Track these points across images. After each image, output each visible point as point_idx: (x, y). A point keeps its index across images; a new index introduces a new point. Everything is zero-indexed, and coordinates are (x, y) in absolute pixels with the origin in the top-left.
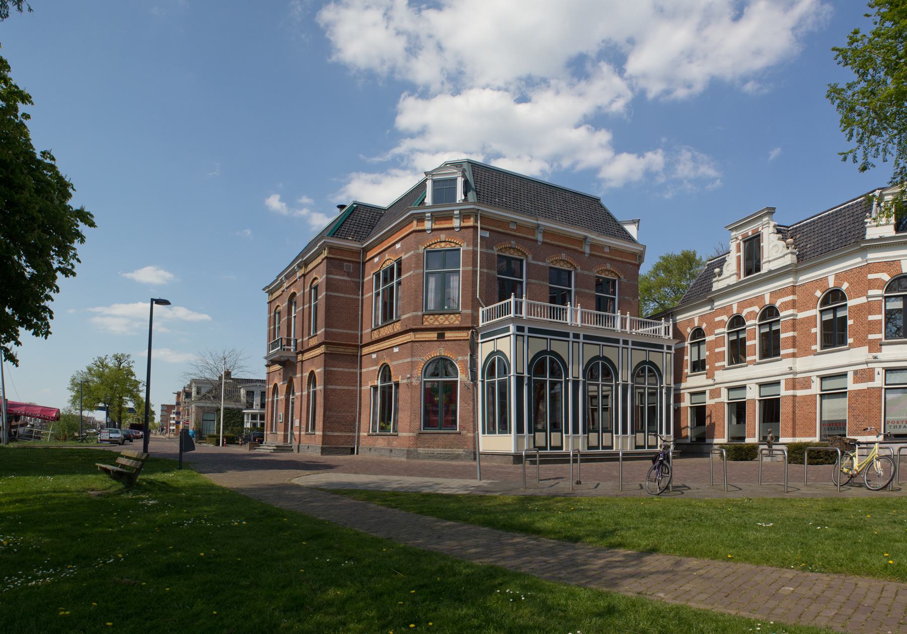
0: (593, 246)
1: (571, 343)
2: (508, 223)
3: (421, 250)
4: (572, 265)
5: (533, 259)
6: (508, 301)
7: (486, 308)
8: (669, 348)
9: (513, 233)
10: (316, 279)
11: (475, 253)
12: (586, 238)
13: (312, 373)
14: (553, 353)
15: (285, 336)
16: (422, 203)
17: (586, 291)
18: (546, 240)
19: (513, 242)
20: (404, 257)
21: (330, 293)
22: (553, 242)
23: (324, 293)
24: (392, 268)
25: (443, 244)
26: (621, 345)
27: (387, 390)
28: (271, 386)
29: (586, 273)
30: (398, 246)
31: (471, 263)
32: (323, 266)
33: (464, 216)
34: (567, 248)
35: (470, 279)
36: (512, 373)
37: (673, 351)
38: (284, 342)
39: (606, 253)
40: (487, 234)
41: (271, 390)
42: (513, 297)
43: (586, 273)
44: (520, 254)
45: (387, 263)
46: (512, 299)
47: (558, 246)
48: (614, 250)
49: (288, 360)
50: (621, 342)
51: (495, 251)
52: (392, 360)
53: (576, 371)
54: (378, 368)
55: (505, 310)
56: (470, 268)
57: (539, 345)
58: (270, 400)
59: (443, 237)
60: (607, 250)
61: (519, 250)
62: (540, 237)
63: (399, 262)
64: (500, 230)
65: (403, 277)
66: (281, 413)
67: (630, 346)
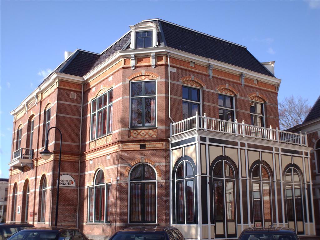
0: (247, 80)
1: (239, 150)
2: (188, 63)
3: (128, 82)
4: (233, 93)
5: (207, 88)
6: (193, 117)
7: (175, 124)
8: (306, 154)
9: (192, 70)
10: (49, 104)
11: (166, 83)
12: (241, 75)
13: (44, 177)
14: (227, 158)
15: (25, 147)
16: (128, 47)
17: (244, 111)
18: (215, 75)
19: (193, 76)
20: (115, 87)
21: (59, 115)
22: (220, 77)
23: (55, 115)
24: (105, 96)
25: (143, 78)
26: (239, 147)
27: (101, 190)
28: (13, 184)
29: (243, 98)
30: (110, 79)
31: (164, 91)
32: (55, 95)
33: (158, 57)
34: (229, 81)
35: (164, 103)
36: (198, 174)
37: (309, 156)
38: (24, 152)
39: (255, 84)
40: (174, 70)
41: (12, 188)
42: (197, 115)
43: (243, 98)
44: (197, 85)
45: (102, 92)
46: (196, 117)
47: (223, 80)
48: (260, 83)
49: (26, 166)
50: (239, 144)
51: (180, 83)
52: (105, 166)
53: (244, 172)
54: (94, 172)
55: (190, 125)
56: (164, 95)
57: (216, 152)
58: (12, 195)
59: (143, 72)
60: (256, 83)
61: (197, 82)
62: (211, 73)
63: (111, 93)
64: (183, 67)
65: (114, 102)
66: (19, 206)
67: (247, 148)
